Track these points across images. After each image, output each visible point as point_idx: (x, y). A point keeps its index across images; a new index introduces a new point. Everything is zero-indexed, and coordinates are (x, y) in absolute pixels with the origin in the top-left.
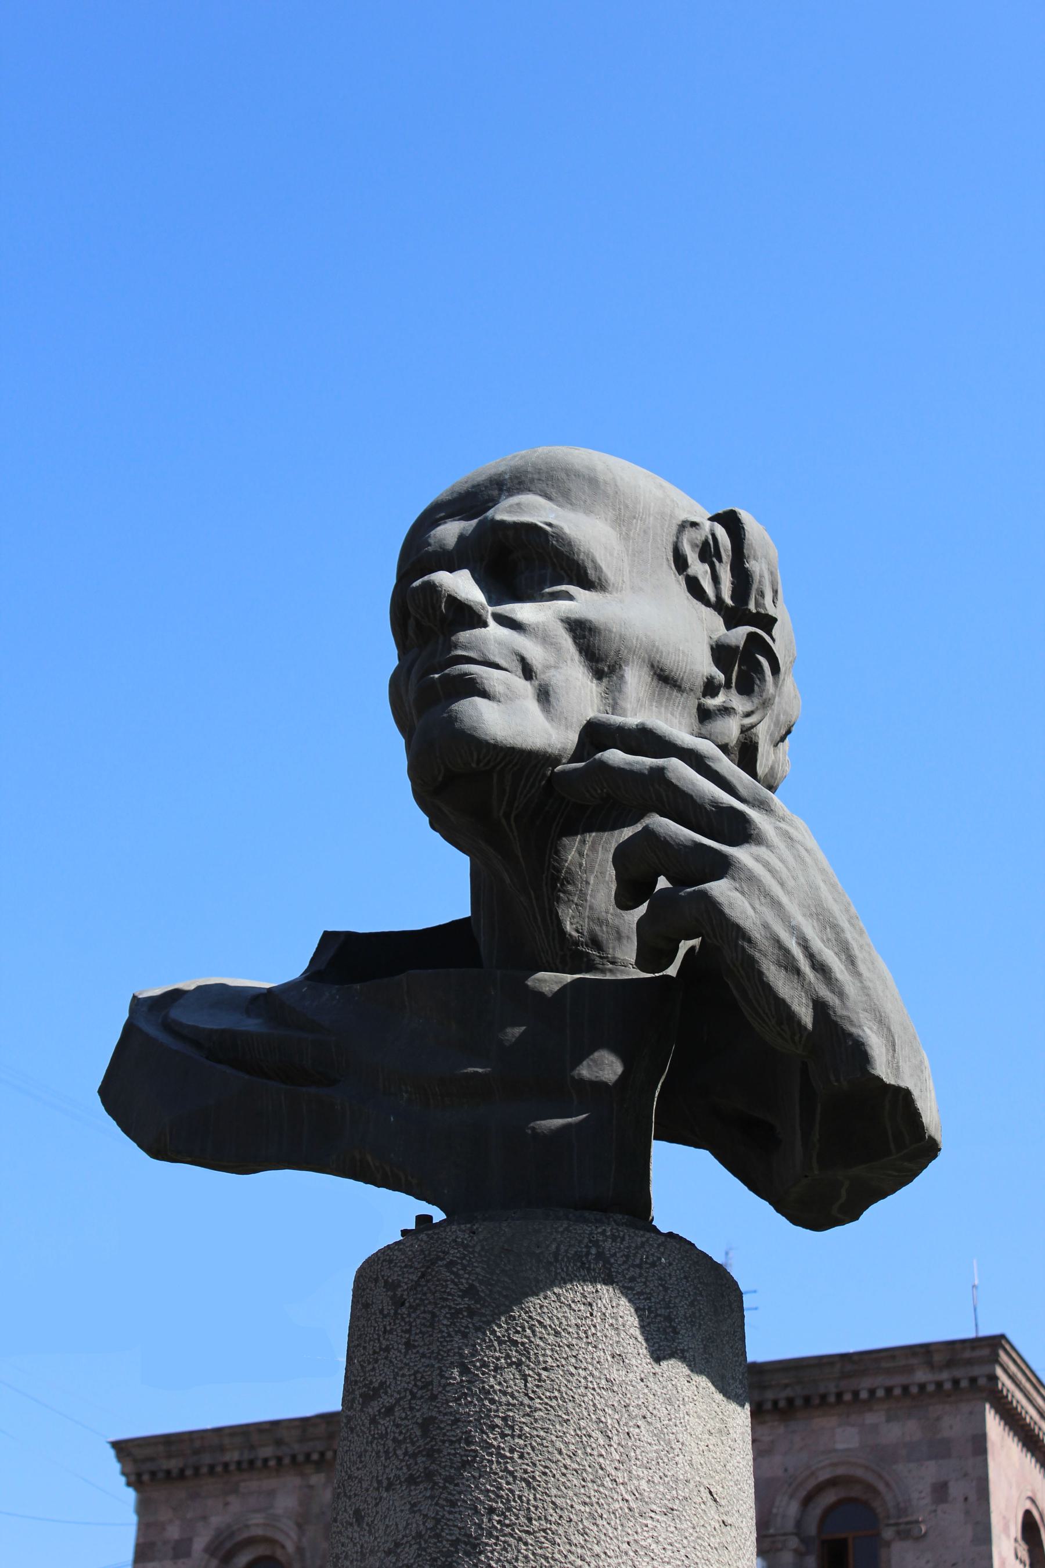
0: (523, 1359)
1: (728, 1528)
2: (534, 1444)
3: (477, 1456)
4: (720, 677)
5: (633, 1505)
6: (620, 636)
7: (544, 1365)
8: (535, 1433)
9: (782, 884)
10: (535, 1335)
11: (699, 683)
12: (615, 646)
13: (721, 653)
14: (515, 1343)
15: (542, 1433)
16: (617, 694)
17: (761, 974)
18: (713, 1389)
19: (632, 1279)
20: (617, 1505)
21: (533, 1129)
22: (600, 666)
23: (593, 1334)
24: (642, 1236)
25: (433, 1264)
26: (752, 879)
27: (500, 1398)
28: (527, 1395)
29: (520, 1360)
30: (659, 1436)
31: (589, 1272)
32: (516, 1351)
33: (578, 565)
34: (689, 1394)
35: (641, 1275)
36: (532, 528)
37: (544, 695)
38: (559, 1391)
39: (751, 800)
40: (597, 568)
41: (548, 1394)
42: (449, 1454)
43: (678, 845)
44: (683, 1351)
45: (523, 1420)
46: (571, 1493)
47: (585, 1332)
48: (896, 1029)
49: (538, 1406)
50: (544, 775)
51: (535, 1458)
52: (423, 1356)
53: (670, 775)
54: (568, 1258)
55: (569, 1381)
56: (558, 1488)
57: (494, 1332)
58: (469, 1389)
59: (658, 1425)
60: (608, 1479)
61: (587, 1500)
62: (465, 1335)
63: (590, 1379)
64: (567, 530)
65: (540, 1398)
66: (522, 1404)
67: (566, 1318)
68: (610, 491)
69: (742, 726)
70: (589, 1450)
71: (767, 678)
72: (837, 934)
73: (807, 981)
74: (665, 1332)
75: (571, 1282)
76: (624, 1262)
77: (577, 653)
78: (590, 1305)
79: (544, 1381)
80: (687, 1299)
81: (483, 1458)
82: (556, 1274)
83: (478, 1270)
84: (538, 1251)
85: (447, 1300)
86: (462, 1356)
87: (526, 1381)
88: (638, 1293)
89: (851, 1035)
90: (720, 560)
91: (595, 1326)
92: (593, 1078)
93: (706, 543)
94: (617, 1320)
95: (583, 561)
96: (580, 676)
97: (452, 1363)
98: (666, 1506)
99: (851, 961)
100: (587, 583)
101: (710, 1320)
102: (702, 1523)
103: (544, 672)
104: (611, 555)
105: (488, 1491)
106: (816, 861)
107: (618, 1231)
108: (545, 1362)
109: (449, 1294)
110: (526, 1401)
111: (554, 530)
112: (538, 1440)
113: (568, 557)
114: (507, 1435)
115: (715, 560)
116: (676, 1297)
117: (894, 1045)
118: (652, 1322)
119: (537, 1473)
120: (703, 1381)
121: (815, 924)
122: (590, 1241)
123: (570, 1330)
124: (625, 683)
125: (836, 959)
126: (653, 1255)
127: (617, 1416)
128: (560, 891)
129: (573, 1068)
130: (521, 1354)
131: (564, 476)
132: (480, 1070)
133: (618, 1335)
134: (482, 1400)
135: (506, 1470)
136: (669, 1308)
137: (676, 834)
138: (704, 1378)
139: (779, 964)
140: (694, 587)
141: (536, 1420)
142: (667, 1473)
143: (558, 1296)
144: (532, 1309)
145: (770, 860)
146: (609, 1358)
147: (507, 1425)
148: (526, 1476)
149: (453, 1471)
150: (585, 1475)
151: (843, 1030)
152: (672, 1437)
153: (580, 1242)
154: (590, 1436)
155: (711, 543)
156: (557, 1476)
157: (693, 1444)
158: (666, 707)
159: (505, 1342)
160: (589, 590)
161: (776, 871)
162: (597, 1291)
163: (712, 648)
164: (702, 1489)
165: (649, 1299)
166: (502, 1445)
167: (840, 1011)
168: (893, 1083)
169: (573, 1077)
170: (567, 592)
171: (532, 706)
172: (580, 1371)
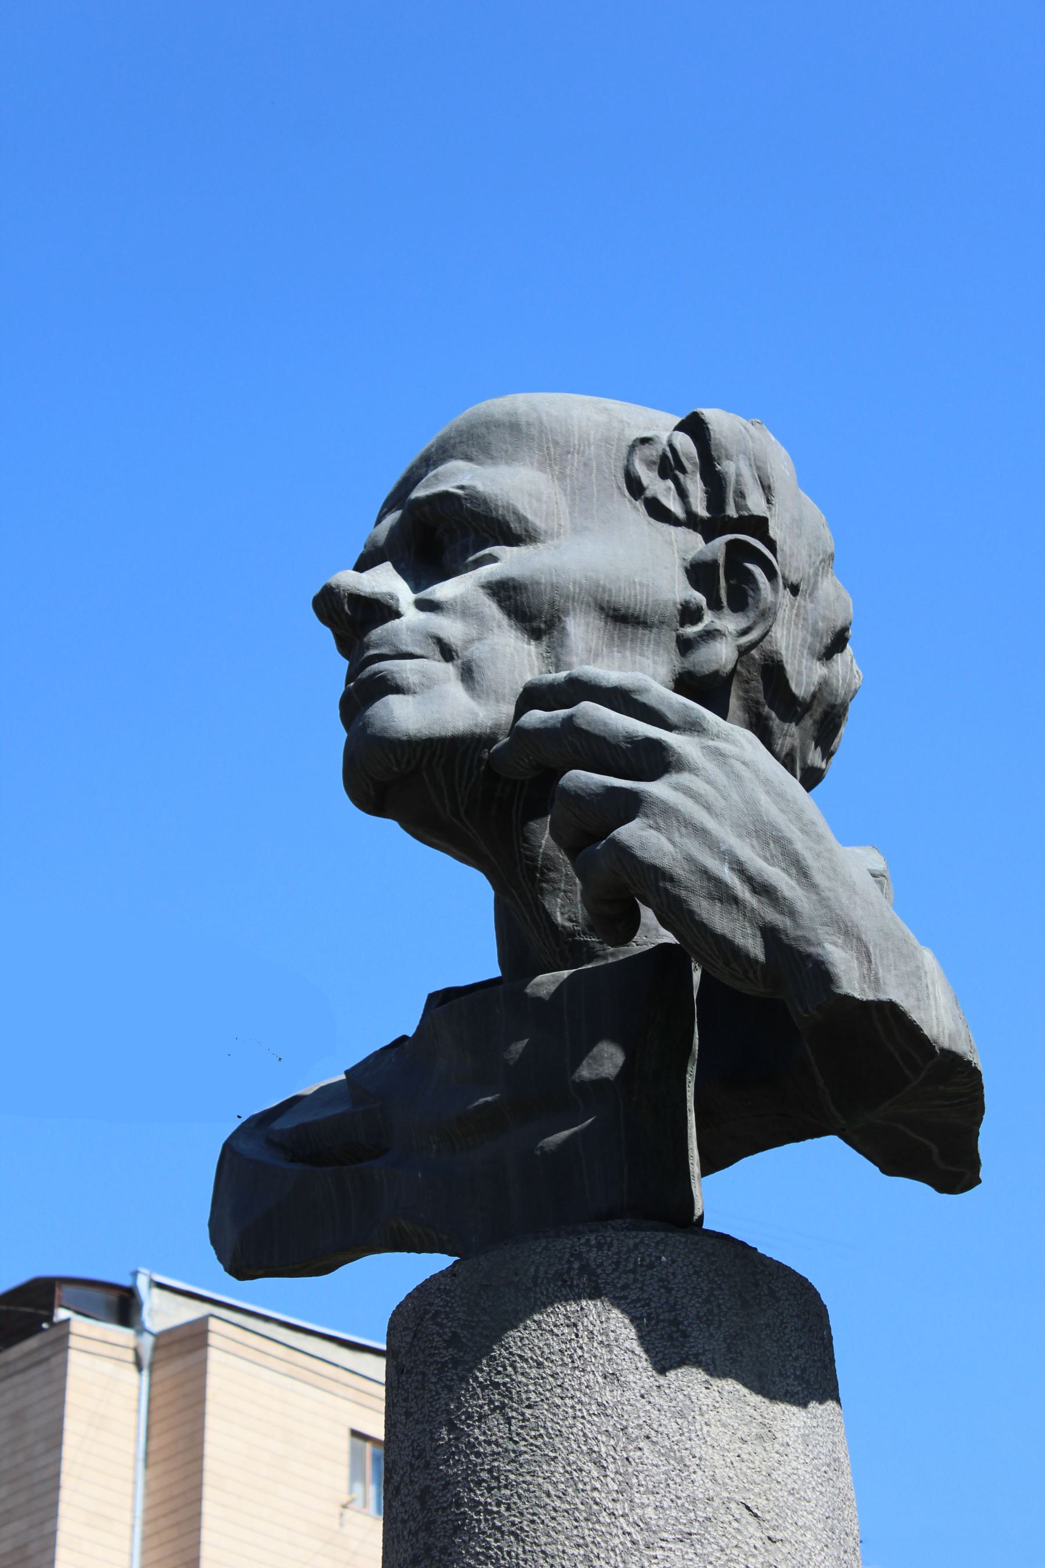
0: (506, 1401)
1: (779, 1544)
2: (521, 1491)
3: (466, 1518)
4: (700, 598)
5: (637, 1537)
6: (552, 585)
7: (527, 1403)
8: (521, 1479)
9: (708, 808)
10: (516, 1372)
11: (673, 612)
12: (546, 598)
13: (699, 573)
14: (496, 1385)
15: (528, 1478)
16: (559, 649)
17: (691, 913)
18: (744, 1391)
19: (625, 1287)
20: (616, 1541)
21: (542, 1148)
22: (535, 624)
23: (580, 1357)
24: (634, 1237)
25: (422, 1320)
26: (668, 811)
27: (485, 1449)
28: (511, 1439)
29: (503, 1403)
30: (667, 1455)
31: (572, 1290)
32: (499, 1394)
33: (499, 521)
34: (709, 1401)
35: (635, 1280)
36: (446, 496)
37: (468, 675)
38: (544, 1427)
39: (680, 724)
40: (521, 519)
41: (533, 1433)
42: (443, 1522)
43: (590, 795)
44: (696, 1355)
45: (508, 1468)
46: (562, 1537)
47: (571, 1356)
48: (870, 937)
49: (523, 1449)
50: (481, 760)
51: (522, 1507)
52: (418, 1422)
53: (580, 722)
54: (548, 1279)
55: (554, 1414)
56: (548, 1535)
57: (476, 1379)
58: (457, 1447)
59: (667, 1443)
60: (604, 1514)
61: (581, 1541)
62: (450, 1389)
63: (578, 1407)
64: (480, 487)
65: (524, 1439)
66: (506, 1450)
67: (548, 1345)
68: (534, 432)
69: (739, 647)
70: (581, 1486)
71: (762, 586)
72: (783, 847)
73: (749, 908)
74: (671, 1337)
75: (552, 1304)
76: (614, 1270)
77: (506, 617)
78: (575, 1325)
79: (528, 1420)
80: (699, 1297)
81: (472, 1519)
82: (536, 1299)
83: (460, 1315)
84: (516, 1279)
85: (434, 1355)
86: (449, 1412)
87: (510, 1424)
88: (633, 1301)
89: (809, 956)
90: (684, 471)
91: (581, 1348)
92: (594, 1077)
93: (664, 457)
94: (607, 1335)
95: (503, 516)
96: (512, 641)
97: (440, 1422)
98: (681, 1532)
99: (802, 873)
100: (513, 539)
101: (736, 1315)
102: (735, 1542)
103: (466, 649)
104: (539, 500)
105: (478, 1553)
106: (756, 772)
107: (604, 1237)
108: (528, 1399)
109: (436, 1348)
110: (511, 1446)
111: (467, 492)
112: (525, 1486)
113: (486, 517)
114: (493, 1488)
115: (677, 473)
116: (682, 1298)
117: (868, 955)
118: (653, 1330)
119: (525, 1523)
120: (730, 1385)
121: (755, 842)
122: (572, 1255)
123: (554, 1358)
124: (568, 635)
125: (784, 876)
126: (650, 1255)
127: (612, 1442)
128: (541, 881)
129: (573, 1072)
130: (504, 1396)
131: (483, 430)
132: (489, 1099)
133: (611, 1352)
134: (468, 1455)
135: (494, 1527)
136: (675, 1310)
137: (586, 784)
138: (730, 1381)
139: (711, 897)
140: (657, 511)
141: (521, 1465)
142: (680, 1494)
143: (538, 1323)
144: (512, 1344)
145: (692, 785)
146: (600, 1380)
147: (493, 1477)
148: (513, 1529)
149: (446, 1540)
150: (577, 1514)
151: (800, 953)
152: (685, 1453)
153: (560, 1259)
154: (581, 1470)
155: (669, 455)
156: (547, 1521)
157: (716, 1457)
158: (632, 650)
159: (487, 1387)
160: (517, 545)
161: (700, 795)
162: (582, 1309)
163: (687, 571)
164: (733, 1505)
165: (648, 1305)
166: (489, 1500)
167: (792, 932)
168: (871, 997)
169: (574, 1081)
170: (490, 555)
171: (455, 690)
172: (567, 1401)
